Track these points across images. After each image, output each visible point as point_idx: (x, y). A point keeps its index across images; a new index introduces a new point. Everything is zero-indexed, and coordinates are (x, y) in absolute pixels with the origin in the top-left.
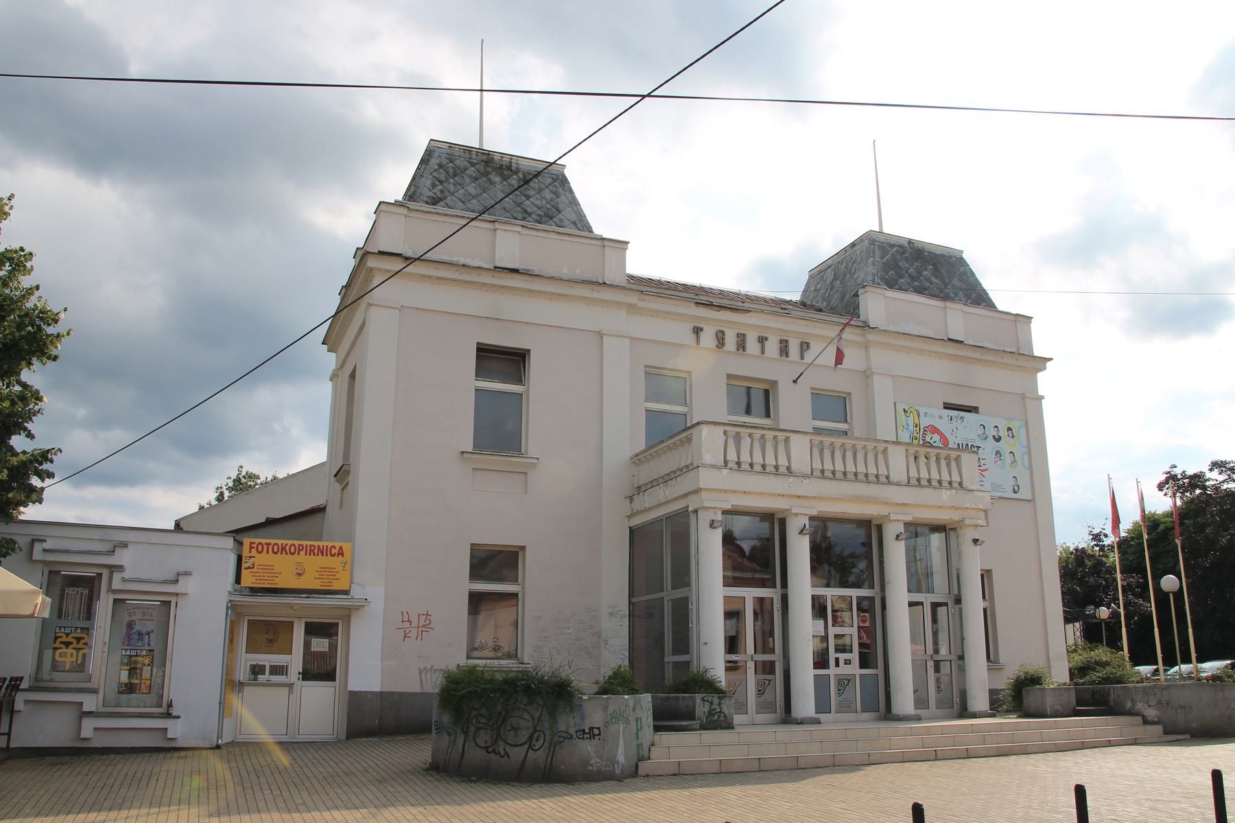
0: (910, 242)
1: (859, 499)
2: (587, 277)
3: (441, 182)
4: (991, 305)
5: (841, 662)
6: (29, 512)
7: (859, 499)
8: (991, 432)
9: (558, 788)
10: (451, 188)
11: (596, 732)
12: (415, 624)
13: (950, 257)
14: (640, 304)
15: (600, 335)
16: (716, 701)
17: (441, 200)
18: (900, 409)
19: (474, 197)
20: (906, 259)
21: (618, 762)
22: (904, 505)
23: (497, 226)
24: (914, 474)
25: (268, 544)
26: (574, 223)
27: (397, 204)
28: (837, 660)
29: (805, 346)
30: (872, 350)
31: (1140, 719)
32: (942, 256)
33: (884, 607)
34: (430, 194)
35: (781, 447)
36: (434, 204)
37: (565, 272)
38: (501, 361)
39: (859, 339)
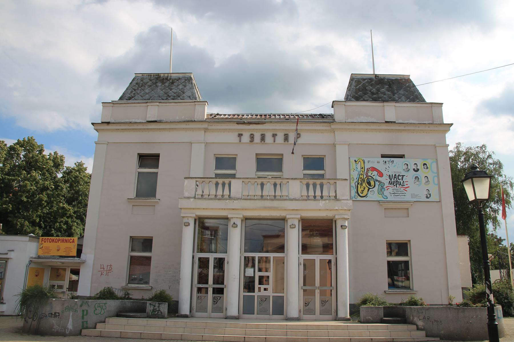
1: (265, 208)
2: (187, 119)
3: (135, 90)
4: (422, 100)
5: (262, 289)
7: (265, 208)
8: (412, 167)
9: (39, 336)
10: (139, 92)
11: (57, 314)
12: (106, 269)
13: (401, 80)
14: (210, 127)
15: (191, 143)
16: (157, 305)
17: (133, 97)
18: (352, 160)
19: (147, 94)
20: (372, 85)
21: (68, 329)
22: (297, 210)
23: (148, 104)
25: (48, 239)
26: (190, 97)
27: (113, 103)
28: (259, 288)
29: (299, 136)
30: (336, 132)
31: (415, 327)
32: (396, 80)
34: (130, 96)
35: (227, 186)
36: (129, 100)
37: (177, 118)
38: (149, 160)
39: (329, 128)
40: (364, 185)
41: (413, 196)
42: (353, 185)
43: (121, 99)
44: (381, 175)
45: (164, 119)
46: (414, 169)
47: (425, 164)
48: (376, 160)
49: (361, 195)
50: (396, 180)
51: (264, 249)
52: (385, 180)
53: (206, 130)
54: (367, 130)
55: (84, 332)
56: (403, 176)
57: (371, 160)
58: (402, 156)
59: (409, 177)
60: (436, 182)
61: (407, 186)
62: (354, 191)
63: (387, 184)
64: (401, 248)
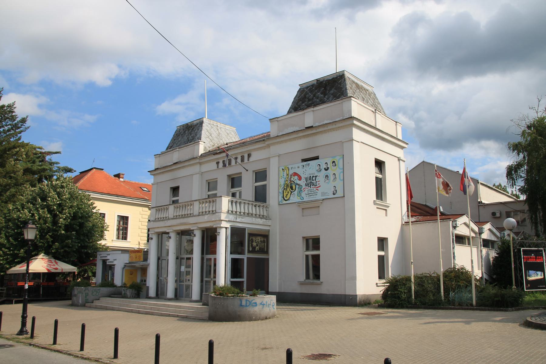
0: (317, 80)
6: (103, 242)
14: (201, 161)
24: (230, 209)
27: (163, 153)
29: (249, 156)
32: (333, 78)
33: (215, 265)
40: (288, 190)
41: (323, 194)
42: (281, 191)
43: (167, 149)
44: (300, 178)
45: (181, 160)
46: (325, 169)
47: (334, 162)
48: (296, 166)
49: (286, 199)
50: (311, 182)
51: (141, 254)
52: (302, 183)
53: (200, 164)
54: (290, 140)
55: (87, 304)
56: (316, 176)
57: (293, 166)
58: (317, 158)
59: (321, 178)
60: (342, 178)
61: (318, 186)
62: (281, 196)
63: (304, 186)
64: (314, 243)
